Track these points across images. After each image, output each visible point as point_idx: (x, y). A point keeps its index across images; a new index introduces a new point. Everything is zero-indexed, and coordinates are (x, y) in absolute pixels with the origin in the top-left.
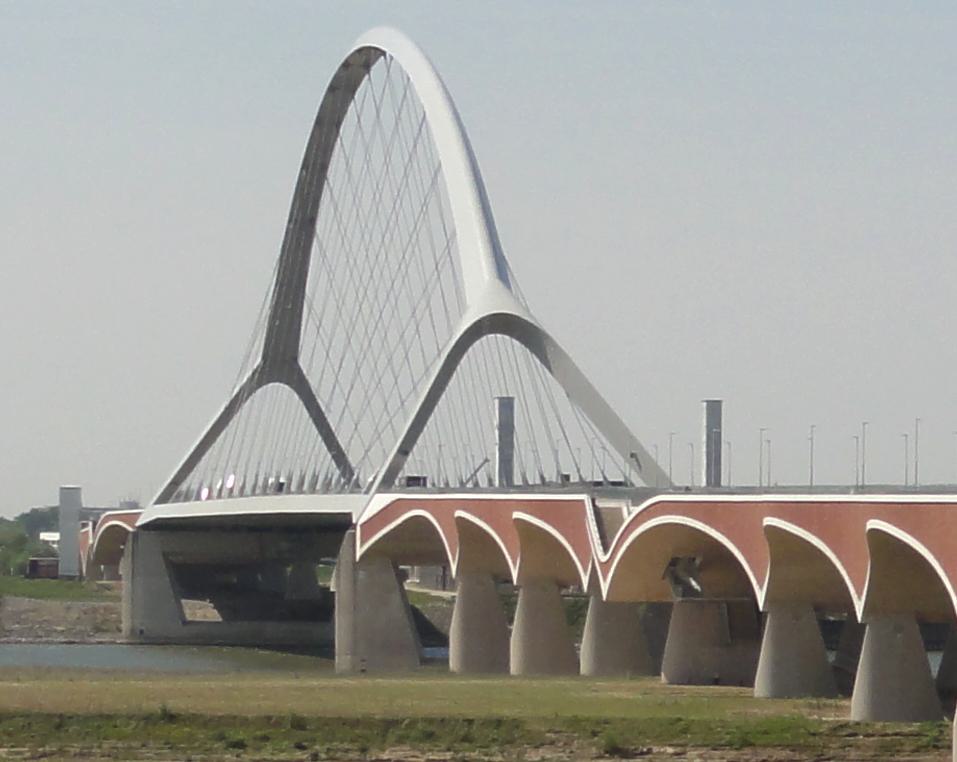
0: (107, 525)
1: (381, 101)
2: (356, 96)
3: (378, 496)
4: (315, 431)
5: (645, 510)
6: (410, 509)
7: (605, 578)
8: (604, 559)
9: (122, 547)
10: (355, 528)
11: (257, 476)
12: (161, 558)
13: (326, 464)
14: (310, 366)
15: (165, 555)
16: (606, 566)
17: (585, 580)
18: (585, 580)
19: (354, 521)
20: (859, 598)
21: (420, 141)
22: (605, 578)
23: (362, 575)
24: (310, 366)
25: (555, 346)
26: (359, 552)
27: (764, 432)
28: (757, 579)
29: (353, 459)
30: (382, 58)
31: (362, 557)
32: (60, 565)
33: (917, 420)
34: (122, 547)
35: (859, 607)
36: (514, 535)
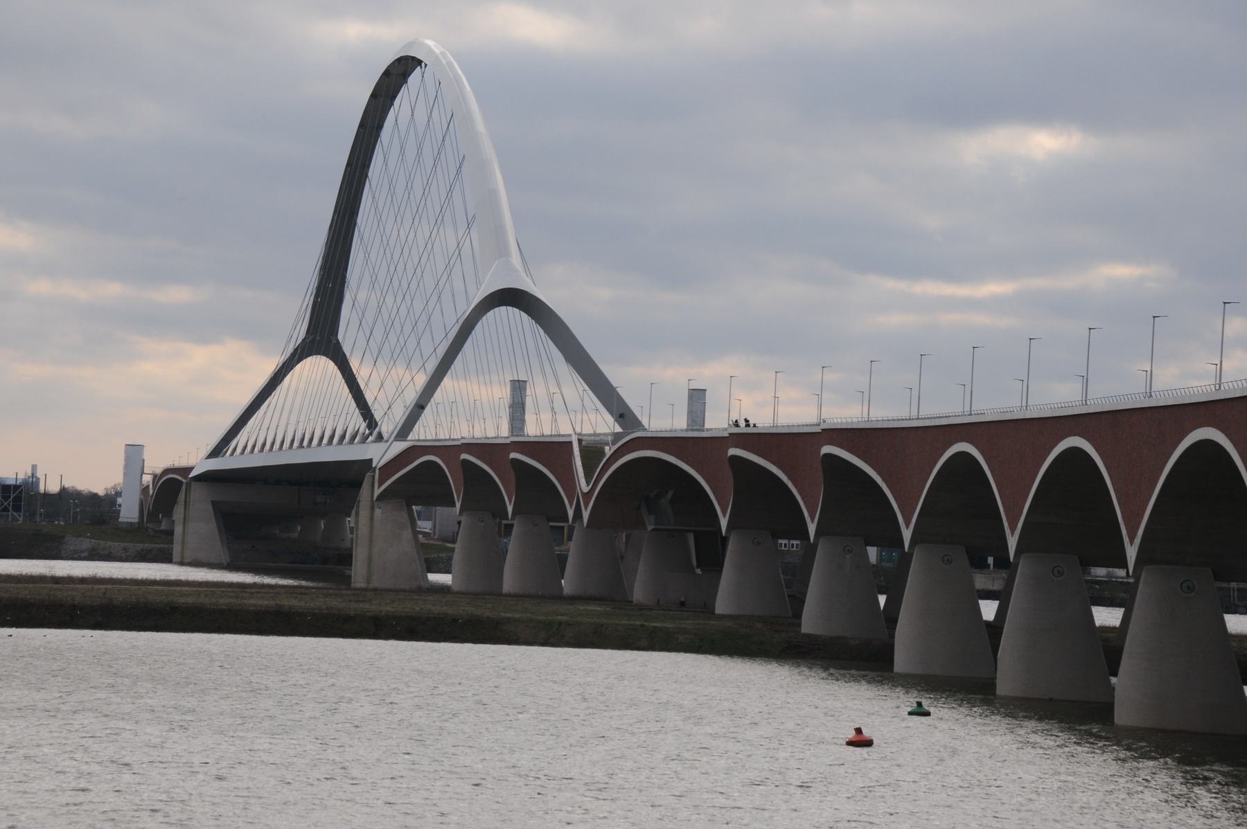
0: (163, 480)
1: (415, 106)
2: (395, 103)
3: (395, 443)
4: (346, 390)
5: (619, 448)
6: (429, 454)
7: (586, 508)
8: (586, 489)
9: (990, 560)
10: (374, 471)
11: (356, 423)
12: (210, 507)
13: (358, 423)
14: (344, 336)
15: (213, 503)
16: (587, 496)
17: (571, 513)
18: (571, 513)
19: (374, 466)
20: (571, 507)
21: (448, 137)
22: (586, 508)
23: (378, 512)
24: (344, 336)
25: (8, 478)
26: (377, 492)
27: (778, 374)
28: (569, 502)
29: (377, 415)
30: (419, 67)
31: (378, 496)
32: (121, 513)
33: (180, 457)
34: (990, 560)
35: (724, 522)
36: (728, 474)
